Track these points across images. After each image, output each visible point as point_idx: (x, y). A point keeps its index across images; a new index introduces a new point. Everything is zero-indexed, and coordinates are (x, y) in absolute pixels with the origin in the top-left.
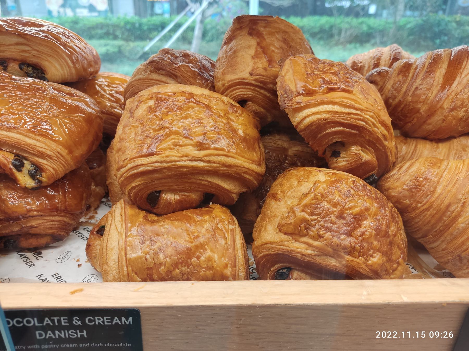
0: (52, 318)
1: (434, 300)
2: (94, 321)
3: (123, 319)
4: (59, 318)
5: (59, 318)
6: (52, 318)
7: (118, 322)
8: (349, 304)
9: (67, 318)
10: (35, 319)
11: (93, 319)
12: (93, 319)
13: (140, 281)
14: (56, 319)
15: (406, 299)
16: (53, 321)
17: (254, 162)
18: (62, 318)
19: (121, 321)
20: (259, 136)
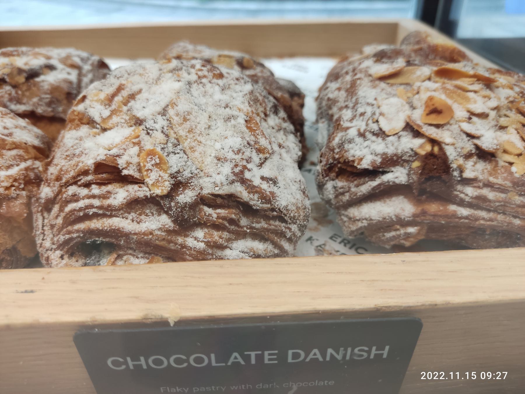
0: (246, 353)
1: (399, 304)
2: (187, 361)
3: (330, 351)
4: (260, 352)
5: (260, 352)
6: (246, 353)
7: (240, 360)
8: (210, 317)
9: (276, 352)
10: (213, 356)
11: (121, 360)
12: (121, 360)
13: (191, 261)
14: (253, 354)
15: (132, 312)
16: (247, 359)
17: (43, 81)
18: (266, 353)
19: (324, 355)
20: (432, 44)
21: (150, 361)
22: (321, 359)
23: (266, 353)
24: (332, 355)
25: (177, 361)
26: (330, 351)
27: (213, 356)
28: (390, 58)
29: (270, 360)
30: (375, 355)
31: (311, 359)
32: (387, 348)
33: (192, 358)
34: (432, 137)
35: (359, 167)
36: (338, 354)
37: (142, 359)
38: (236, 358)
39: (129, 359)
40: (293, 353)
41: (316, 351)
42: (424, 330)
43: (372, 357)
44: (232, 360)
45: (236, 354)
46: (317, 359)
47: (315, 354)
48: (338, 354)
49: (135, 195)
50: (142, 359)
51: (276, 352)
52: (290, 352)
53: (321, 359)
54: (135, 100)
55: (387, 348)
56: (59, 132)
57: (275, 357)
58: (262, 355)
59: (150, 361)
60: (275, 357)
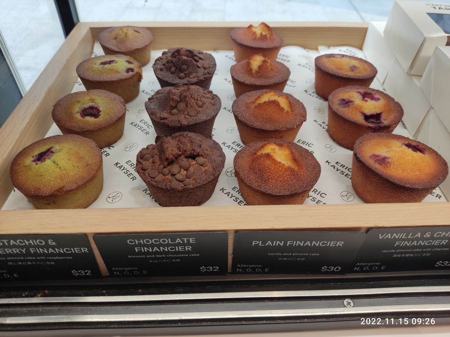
2: (159, 241)
3: (314, 242)
7: (180, 241)
10: (169, 240)
14: (185, 239)
18: (191, 239)
21: (64, 250)
22: (46, 252)
23: (191, 239)
26: (314, 242)
32: (288, 245)
35: (238, 187)
37: (141, 240)
39: (136, 240)
41: (269, 242)
45: (178, 239)
52: (254, 242)
54: (339, 104)
55: (288, 245)
59: (64, 250)
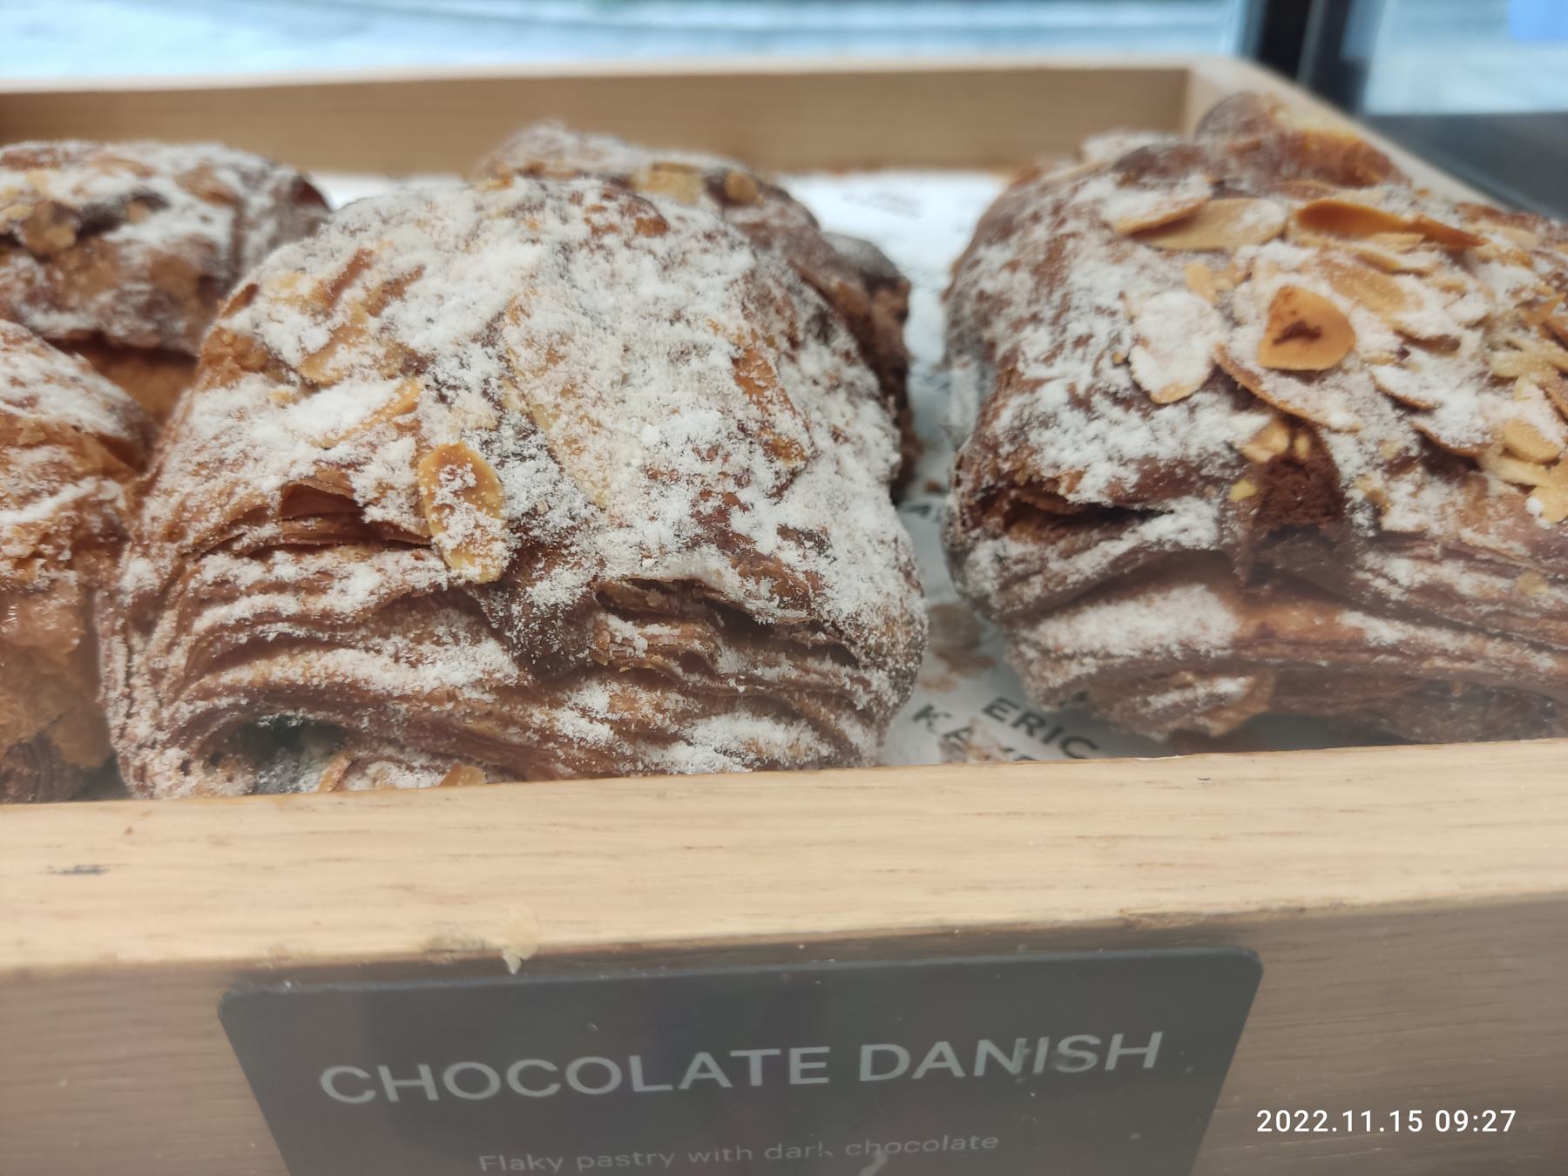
0: (734, 1054)
2: (560, 1077)
3: (985, 1047)
4: (776, 1052)
5: (776, 1052)
6: (734, 1054)
7: (717, 1074)
9: (825, 1050)
14: (755, 1057)
16: (738, 1070)
22: (958, 1072)
24: (991, 1060)
25: (528, 1077)
26: (985, 1047)
27: (635, 1063)
28: (1164, 172)
29: (806, 1073)
30: (1121, 1058)
31: (929, 1071)
33: (574, 1067)
34: (1290, 408)
36: (1010, 1056)
37: (425, 1070)
38: (704, 1068)
39: (384, 1072)
40: (876, 1054)
42: (1265, 984)
43: (1111, 1064)
44: (692, 1073)
46: (948, 1071)
47: (941, 1058)
48: (1010, 1056)
49: (404, 582)
50: (425, 1070)
51: (825, 1050)
53: (958, 1072)
56: (175, 395)
57: (822, 1065)
58: (784, 1061)
60: (822, 1065)
